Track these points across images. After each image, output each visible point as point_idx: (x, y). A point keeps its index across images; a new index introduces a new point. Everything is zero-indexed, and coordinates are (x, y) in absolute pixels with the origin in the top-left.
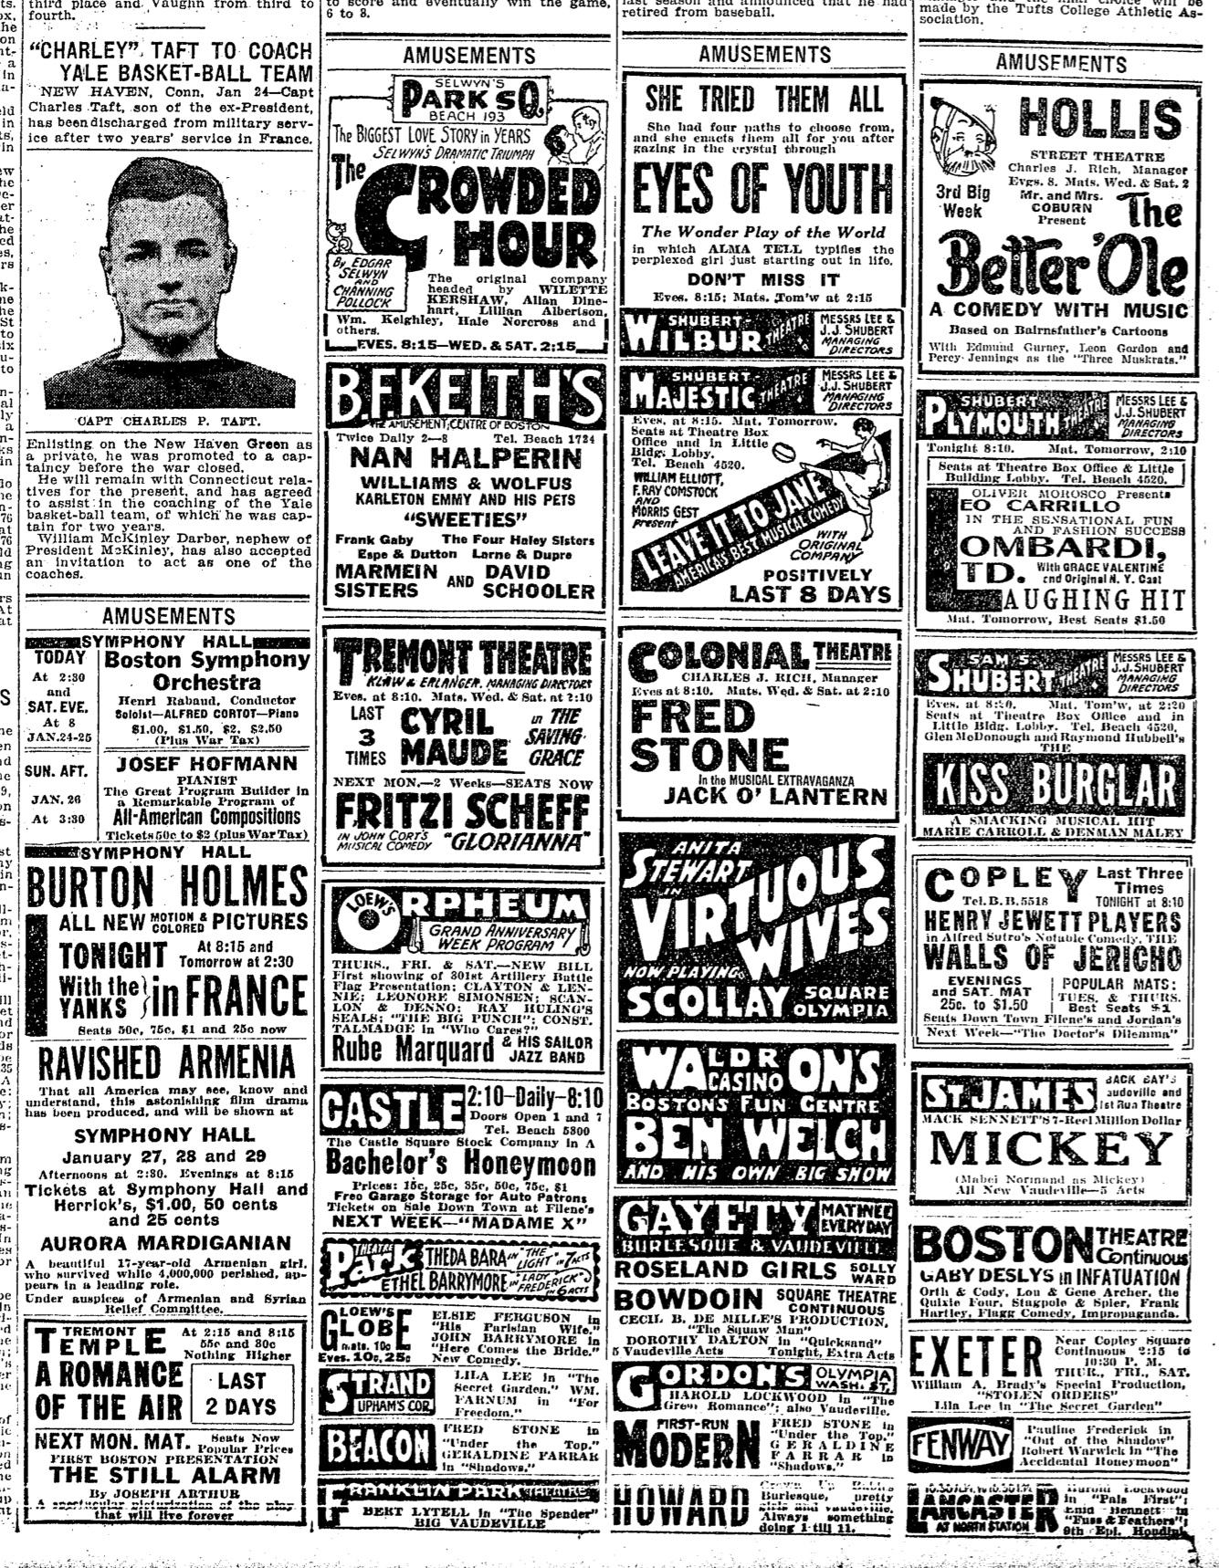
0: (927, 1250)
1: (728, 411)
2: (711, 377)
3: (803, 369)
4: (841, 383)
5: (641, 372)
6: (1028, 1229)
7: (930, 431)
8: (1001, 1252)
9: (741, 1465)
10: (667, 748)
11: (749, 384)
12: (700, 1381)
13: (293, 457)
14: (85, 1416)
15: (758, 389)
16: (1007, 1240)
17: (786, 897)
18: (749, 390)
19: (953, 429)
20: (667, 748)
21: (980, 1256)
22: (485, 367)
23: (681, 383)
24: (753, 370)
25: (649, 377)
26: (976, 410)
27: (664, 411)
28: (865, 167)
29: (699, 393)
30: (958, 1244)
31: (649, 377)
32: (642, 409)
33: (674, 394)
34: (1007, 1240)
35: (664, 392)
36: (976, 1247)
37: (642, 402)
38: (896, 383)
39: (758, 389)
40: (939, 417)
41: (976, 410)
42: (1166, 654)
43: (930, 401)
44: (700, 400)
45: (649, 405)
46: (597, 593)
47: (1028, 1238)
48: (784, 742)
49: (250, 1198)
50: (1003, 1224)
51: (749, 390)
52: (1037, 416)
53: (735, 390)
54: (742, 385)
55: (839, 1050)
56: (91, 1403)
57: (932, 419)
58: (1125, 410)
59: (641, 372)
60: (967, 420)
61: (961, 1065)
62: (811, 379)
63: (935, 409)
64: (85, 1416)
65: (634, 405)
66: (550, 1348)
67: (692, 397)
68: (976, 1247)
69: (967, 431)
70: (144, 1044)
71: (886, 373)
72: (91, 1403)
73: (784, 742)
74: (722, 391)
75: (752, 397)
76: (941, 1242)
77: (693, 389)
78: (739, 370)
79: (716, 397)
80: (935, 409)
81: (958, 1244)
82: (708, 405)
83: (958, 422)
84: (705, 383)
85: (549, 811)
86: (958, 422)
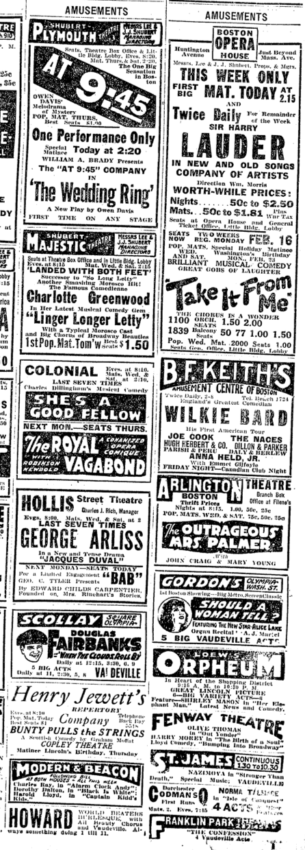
1: (73, 252)
2: (65, 237)
3: (110, 234)
4: (127, 241)
5: (33, 233)
7: (35, 38)
11: (83, 240)
12: (193, 672)
13: (168, 737)
14: (183, 78)
15: (88, 242)
18: (83, 243)
19: (46, 38)
23: (51, 239)
24: (85, 234)
25: (36, 235)
26: (57, 29)
27: (43, 252)
29: (59, 244)
31: (36, 235)
32: (32, 250)
33: (48, 244)
35: (43, 243)
37: (32, 247)
38: (153, 241)
39: (88, 242)
40: (39, 32)
41: (57, 29)
42: (144, 235)
43: (36, 24)
44: (60, 247)
45: (36, 249)
48: (282, 723)
51: (83, 243)
52: (85, 34)
53: (77, 243)
54: (79, 240)
55: (129, 475)
57: (36, 33)
58: (128, 31)
59: (33, 233)
60: (52, 34)
62: (113, 239)
63: (38, 28)
64: (183, 78)
65: (28, 248)
67: (56, 246)
69: (52, 39)
71: (148, 236)
73: (282, 723)
74: (71, 243)
75: (84, 246)
77: (56, 242)
78: (79, 233)
79: (67, 245)
80: (38, 28)
82: (64, 249)
83: (48, 34)
84: (62, 239)
86: (48, 34)
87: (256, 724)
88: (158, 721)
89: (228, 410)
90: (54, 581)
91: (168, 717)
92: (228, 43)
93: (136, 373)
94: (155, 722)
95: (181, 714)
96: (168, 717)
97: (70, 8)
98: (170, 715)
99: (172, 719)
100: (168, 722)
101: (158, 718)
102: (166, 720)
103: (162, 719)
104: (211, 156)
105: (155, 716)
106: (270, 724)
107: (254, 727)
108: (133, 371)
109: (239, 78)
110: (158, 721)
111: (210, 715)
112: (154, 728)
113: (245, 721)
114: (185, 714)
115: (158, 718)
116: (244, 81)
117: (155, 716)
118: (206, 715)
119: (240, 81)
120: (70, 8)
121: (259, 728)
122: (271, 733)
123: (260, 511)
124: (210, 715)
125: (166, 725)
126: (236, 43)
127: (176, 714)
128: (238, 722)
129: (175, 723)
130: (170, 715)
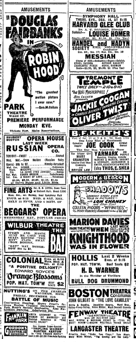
0: (72, 294)
6: (94, 290)
8: (88, 295)
9: (111, 327)
10: (90, 291)
16: (90, 292)
17: (47, 70)
20: (90, 291)
21: (84, 296)
22: (105, 130)
28: (107, 326)
30: (79, 293)
34: (90, 292)
36: (83, 294)
46: (64, 284)
47: (94, 292)
49: (44, 310)
50: (89, 289)
56: (107, 328)
61: (135, 168)
66: (60, 309)
68: (83, 294)
70: (99, 326)
72: (107, 328)
76: (75, 292)
81: (79, 293)
85: (98, 328)
87: (118, 313)
88: (72, 315)
89: (16, 188)
90: (14, 291)
91: (77, 313)
92: (51, 212)
93: (58, 261)
94: (70, 315)
95: (83, 311)
96: (77, 313)
97: (89, 9)
98: (78, 311)
99: (78, 314)
100: (77, 315)
101: (72, 313)
102: (75, 314)
103: (73, 314)
104: (70, 234)
105: (70, 312)
106: (125, 313)
107: (117, 315)
108: (57, 260)
109: (55, 213)
110: (72, 315)
111: (97, 311)
112: (70, 317)
113: (113, 312)
114: (85, 311)
115: (72, 313)
116: (58, 215)
117: (70, 312)
118: (94, 311)
119: (56, 215)
120: (89, 9)
121: (120, 315)
122: (126, 317)
123: (22, 196)
124: (97, 311)
125: (75, 316)
126: (55, 212)
127: (80, 311)
128: (110, 313)
129: (80, 315)
130: (78, 311)
